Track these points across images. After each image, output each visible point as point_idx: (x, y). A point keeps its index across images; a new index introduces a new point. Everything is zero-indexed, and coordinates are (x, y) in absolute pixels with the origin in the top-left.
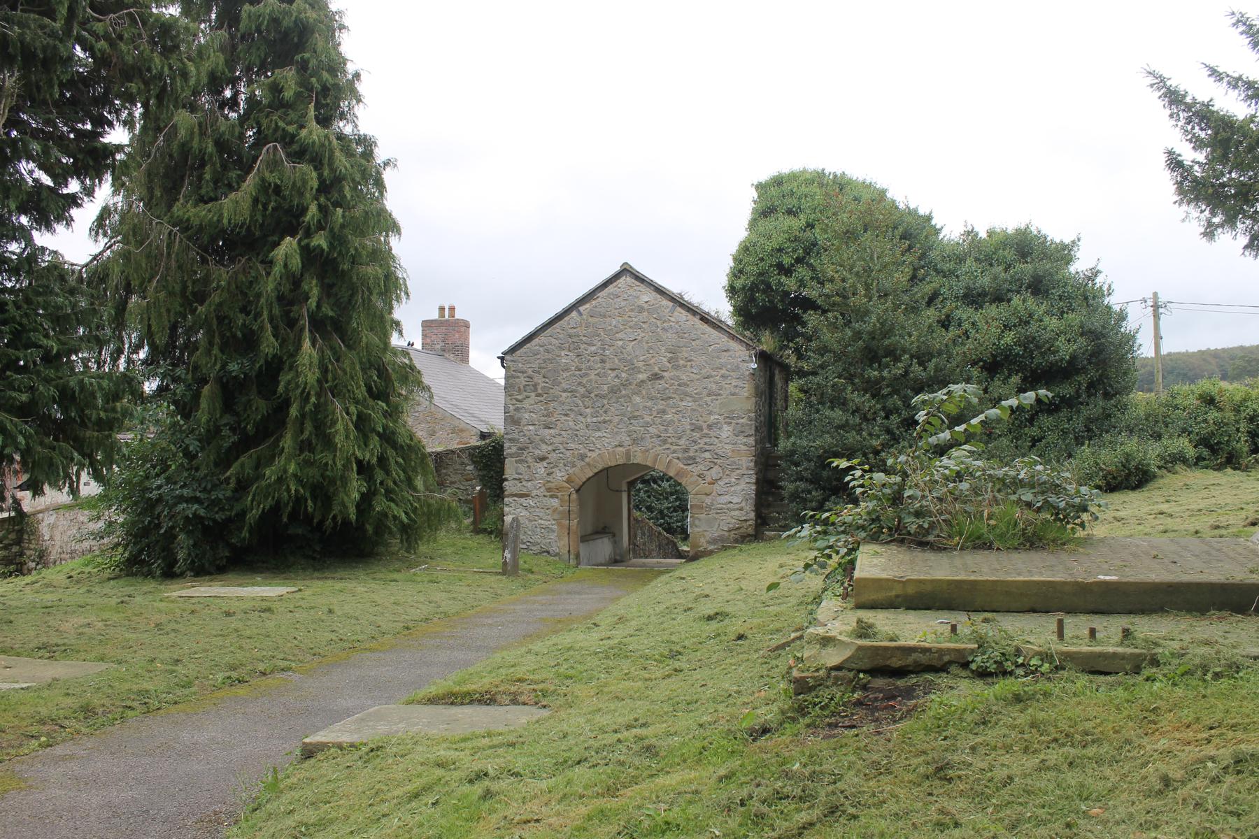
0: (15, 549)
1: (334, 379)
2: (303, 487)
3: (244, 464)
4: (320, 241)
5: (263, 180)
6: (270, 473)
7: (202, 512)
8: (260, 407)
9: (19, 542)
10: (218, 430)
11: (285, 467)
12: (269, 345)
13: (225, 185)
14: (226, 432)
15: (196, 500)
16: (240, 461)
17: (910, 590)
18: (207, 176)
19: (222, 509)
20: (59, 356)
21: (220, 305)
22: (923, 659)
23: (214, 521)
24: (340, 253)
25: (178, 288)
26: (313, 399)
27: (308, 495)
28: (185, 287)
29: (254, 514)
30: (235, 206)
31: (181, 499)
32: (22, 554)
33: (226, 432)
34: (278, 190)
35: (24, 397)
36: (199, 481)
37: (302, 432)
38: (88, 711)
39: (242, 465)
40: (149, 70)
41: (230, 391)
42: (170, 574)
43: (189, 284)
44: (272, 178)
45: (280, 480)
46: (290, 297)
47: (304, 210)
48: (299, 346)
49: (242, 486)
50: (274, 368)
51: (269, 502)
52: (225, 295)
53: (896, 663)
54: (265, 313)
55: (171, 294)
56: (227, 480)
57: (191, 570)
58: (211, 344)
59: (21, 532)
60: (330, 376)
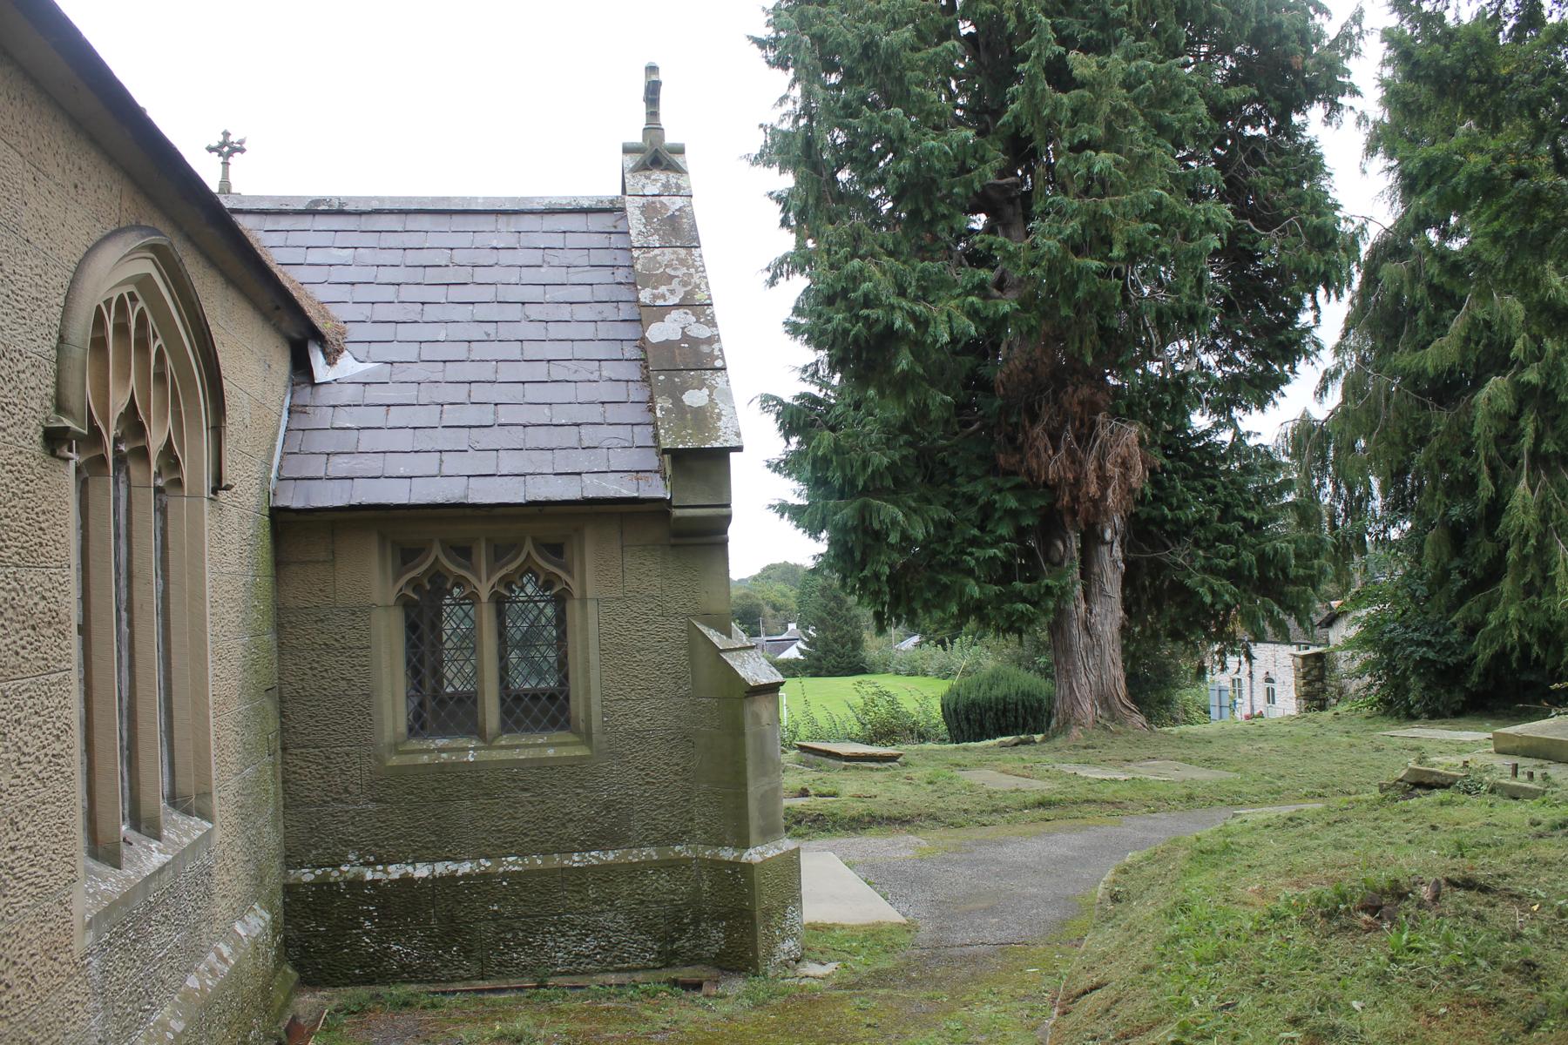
0: (1318, 685)
1: (1559, 517)
2: (1530, 632)
3: (1473, 605)
4: (1532, 376)
5: (1473, 318)
6: (1493, 619)
7: (1431, 655)
8: (1487, 549)
9: (1321, 678)
10: (1446, 573)
11: (1508, 610)
12: (1486, 488)
13: (1437, 326)
14: (1455, 575)
15: (1428, 644)
16: (1466, 607)
17: (1525, 743)
18: (1420, 322)
19: (1454, 653)
20: (1261, 523)
21: (1441, 448)
22: (1439, 779)
23: (1446, 664)
24: (1558, 383)
25: (1397, 439)
26: (1533, 541)
27: (1534, 640)
28: (1405, 435)
29: (1484, 656)
30: (1441, 353)
31: (1412, 642)
32: (1324, 691)
33: (1455, 575)
34: (1488, 325)
35: (1231, 563)
36: (1432, 624)
37: (1525, 573)
38: (1190, 797)
39: (1470, 609)
40: (1307, 271)
41: (1458, 536)
42: (1411, 717)
43: (1410, 432)
44: (1481, 314)
45: (1504, 625)
46: (1507, 436)
47: (1510, 344)
48: (1516, 483)
49: (1472, 630)
50: (1497, 508)
51: (1496, 647)
52: (1446, 438)
53: (1426, 780)
54: (1482, 454)
55: (1392, 444)
56: (1455, 625)
57: (1427, 712)
58: (1435, 488)
59: (1322, 669)
60: (1554, 515)
